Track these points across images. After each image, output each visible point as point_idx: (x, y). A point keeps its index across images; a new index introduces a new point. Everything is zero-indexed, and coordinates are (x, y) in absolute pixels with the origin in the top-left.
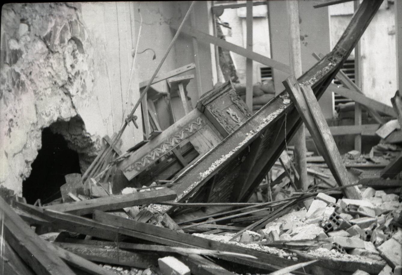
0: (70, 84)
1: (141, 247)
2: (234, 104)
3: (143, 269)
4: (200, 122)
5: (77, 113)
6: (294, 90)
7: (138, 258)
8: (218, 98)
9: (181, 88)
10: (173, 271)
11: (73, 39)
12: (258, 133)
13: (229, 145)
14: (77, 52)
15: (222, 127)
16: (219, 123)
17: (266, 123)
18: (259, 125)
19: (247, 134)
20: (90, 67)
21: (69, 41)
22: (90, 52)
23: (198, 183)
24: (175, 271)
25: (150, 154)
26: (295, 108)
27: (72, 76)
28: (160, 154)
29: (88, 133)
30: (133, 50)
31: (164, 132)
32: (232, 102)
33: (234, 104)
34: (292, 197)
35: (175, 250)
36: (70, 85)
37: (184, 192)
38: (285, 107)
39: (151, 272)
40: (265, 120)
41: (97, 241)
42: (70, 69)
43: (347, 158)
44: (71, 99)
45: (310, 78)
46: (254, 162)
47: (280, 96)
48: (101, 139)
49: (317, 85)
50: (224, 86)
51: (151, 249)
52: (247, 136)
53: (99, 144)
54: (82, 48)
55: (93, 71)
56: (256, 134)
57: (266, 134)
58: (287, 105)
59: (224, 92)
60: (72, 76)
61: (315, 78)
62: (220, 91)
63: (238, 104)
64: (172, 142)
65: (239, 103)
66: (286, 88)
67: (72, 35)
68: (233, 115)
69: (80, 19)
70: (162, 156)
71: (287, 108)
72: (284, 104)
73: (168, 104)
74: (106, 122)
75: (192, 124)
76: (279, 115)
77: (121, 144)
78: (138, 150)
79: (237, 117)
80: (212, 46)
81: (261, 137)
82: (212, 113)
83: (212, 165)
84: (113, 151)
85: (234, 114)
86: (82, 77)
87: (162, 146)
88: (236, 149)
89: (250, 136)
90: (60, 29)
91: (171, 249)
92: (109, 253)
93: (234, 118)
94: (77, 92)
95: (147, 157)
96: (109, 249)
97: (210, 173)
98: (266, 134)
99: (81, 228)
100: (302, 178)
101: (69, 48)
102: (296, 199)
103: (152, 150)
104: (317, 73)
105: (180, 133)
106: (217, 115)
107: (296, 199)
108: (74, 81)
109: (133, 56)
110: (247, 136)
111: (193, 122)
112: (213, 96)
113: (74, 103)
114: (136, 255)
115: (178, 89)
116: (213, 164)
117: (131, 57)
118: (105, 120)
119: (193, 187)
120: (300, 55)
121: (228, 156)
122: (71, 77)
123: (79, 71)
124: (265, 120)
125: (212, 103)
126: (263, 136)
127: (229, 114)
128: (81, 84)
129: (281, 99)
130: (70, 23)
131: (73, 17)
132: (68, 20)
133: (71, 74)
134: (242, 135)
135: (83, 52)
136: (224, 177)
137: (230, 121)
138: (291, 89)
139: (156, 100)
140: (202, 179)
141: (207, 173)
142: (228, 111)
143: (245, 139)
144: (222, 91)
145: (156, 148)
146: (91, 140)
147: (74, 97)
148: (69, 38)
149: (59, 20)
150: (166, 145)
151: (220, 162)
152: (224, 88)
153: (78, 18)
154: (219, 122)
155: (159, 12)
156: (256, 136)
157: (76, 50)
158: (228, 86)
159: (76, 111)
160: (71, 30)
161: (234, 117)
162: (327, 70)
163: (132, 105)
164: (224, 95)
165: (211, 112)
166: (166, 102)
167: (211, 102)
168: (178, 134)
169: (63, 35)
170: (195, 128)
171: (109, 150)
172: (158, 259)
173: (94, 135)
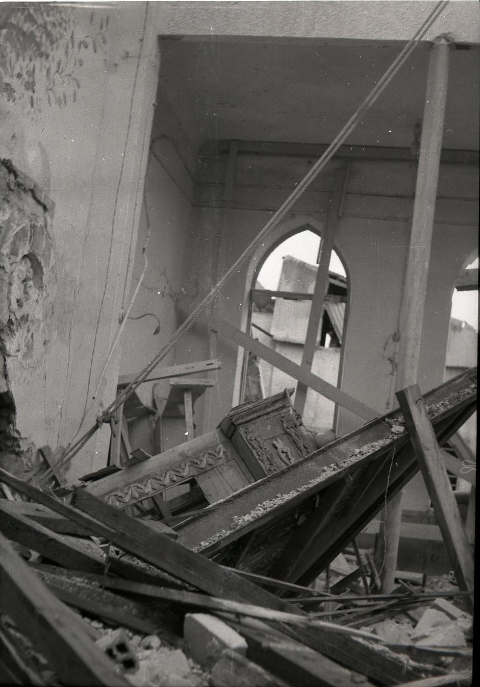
0: (9, 332)
1: (148, 590)
2: (286, 433)
3: (145, 634)
4: (222, 452)
5: (8, 388)
6: (414, 410)
7: (134, 611)
8: (260, 419)
9: (188, 398)
10: (214, 639)
11: (30, 257)
12: (345, 470)
13: (292, 481)
14: (31, 283)
15: (262, 468)
16: (256, 459)
17: (359, 456)
18: (345, 457)
19: (325, 468)
20: (45, 316)
21: (25, 257)
22: (52, 291)
23: (228, 533)
24: (217, 638)
25: (122, 491)
26: (409, 443)
27: (16, 319)
28: (141, 494)
29: (18, 432)
30: (122, 311)
31: (153, 458)
32: (285, 430)
33: (286, 433)
34: (392, 596)
35: (220, 604)
36: (8, 335)
37: (202, 543)
38: (395, 438)
39: (160, 643)
40: (357, 451)
41: (54, 567)
42: (14, 306)
43: (447, 581)
44: (5, 360)
45: (440, 402)
46: (310, 541)
47: (387, 419)
48: (35, 451)
49: (447, 416)
50: (274, 399)
51: (169, 597)
52: (324, 471)
53: (30, 460)
54: (42, 279)
55: (49, 326)
56: (340, 470)
57: (355, 475)
58: (398, 434)
59: (273, 411)
60: (16, 319)
61: (447, 403)
62: (266, 407)
63: (293, 434)
64: (165, 477)
65: (296, 434)
66: (400, 404)
67: (31, 249)
68: (283, 452)
69: (49, 228)
70: (143, 498)
71: (397, 440)
72: (393, 432)
73: (154, 428)
74: (50, 424)
75: (207, 454)
76: (383, 448)
77: (67, 469)
78: (102, 480)
79: (290, 457)
80: (241, 351)
81: (347, 480)
82: (248, 440)
83: (257, 508)
84: (54, 478)
85: (285, 450)
86: (30, 328)
87: (147, 482)
88: (303, 489)
89: (329, 473)
90: (16, 229)
91: (212, 601)
92: (80, 588)
93: (283, 456)
94: (18, 351)
95: (115, 495)
96: (80, 582)
97: (253, 520)
98: (355, 475)
99: (29, 534)
100: (384, 587)
101: (20, 271)
102: (396, 601)
103: (128, 485)
104: (451, 395)
105: (183, 465)
106: (256, 445)
107: (396, 601)
108: (17, 330)
109: (121, 322)
110: (324, 471)
111: (210, 452)
112: (254, 412)
113: (8, 367)
114: (132, 604)
115: (183, 403)
116: (259, 505)
117: (118, 322)
118: (48, 419)
119: (220, 538)
120: (416, 368)
121: (287, 497)
122: (14, 320)
123: (28, 315)
124: (357, 451)
125: (248, 425)
126: (351, 479)
127: (276, 448)
128: (26, 340)
129: (387, 425)
130: (33, 227)
131: (38, 219)
132: (31, 221)
133: (15, 315)
134: (316, 468)
135: (41, 287)
136: (262, 548)
137: (277, 460)
138: (410, 406)
139: (133, 418)
140: (238, 528)
141: (247, 518)
142: (275, 442)
143: (319, 476)
144: (269, 407)
145: (134, 482)
146: (19, 446)
147: (11, 358)
148: (26, 252)
149: (16, 214)
150: (154, 481)
151: (272, 505)
152: (274, 403)
153: (46, 226)
154: (257, 457)
155: (164, 274)
156: (340, 473)
157: (31, 280)
158: (280, 402)
159: (7, 385)
160: (32, 240)
161: (285, 454)
162: (468, 393)
163: (101, 405)
164: (272, 414)
165: (245, 439)
166: (150, 424)
167: (246, 422)
168: (180, 466)
169: (17, 242)
170: (211, 461)
171: (45, 475)
172: (185, 613)
173: (26, 438)
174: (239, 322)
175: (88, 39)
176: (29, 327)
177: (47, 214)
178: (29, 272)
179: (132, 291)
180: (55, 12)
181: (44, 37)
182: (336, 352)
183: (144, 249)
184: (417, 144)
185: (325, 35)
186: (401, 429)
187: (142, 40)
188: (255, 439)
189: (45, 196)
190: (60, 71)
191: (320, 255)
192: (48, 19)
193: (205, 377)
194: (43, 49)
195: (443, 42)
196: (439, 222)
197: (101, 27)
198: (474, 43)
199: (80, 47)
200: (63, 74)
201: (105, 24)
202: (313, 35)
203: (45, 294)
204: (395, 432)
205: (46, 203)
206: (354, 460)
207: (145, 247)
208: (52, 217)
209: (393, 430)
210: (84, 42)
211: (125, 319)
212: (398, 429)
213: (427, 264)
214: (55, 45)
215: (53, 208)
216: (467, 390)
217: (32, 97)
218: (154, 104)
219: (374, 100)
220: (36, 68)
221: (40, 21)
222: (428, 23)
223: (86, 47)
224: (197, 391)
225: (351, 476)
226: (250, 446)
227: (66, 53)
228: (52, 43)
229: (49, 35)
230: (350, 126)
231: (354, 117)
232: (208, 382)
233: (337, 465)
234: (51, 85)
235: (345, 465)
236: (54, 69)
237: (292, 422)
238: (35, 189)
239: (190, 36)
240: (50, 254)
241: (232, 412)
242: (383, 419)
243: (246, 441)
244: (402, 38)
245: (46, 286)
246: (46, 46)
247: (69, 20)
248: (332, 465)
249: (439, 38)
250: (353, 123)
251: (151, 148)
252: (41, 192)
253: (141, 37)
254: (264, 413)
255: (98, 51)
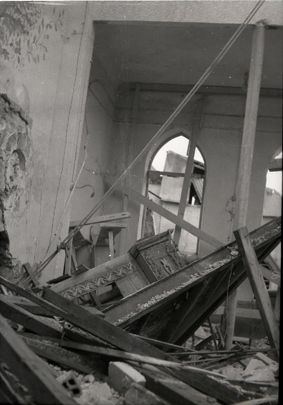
0: (5, 196)
1: (88, 348)
2: (169, 255)
3: (86, 374)
4: (131, 267)
5: (5, 229)
6: (244, 242)
7: (79, 360)
8: (153, 247)
9: (111, 235)
10: (126, 377)
11: (18, 152)
12: (203, 277)
13: (172, 283)
14: (18, 167)
15: (154, 276)
16: (151, 271)
17: (212, 269)
18: (204, 270)
19: (192, 276)
20: (27, 186)
21: (15, 151)
22: (31, 171)
23: (135, 314)
24: (128, 376)
25: (72, 289)
26: (241, 261)
27: (10, 188)
28: (83, 291)
29: (10, 255)
30: (72, 183)
31: (90, 270)
32: (168, 254)
33: (169, 255)
34: (231, 351)
35: (130, 356)
36: (5, 197)
37: (119, 320)
38: (233, 258)
39: (94, 379)
40: (211, 266)
41: (32, 334)
42: (9, 180)
43: (264, 343)
44: (3, 212)
45: (259, 237)
46: (183, 319)
47: (228, 247)
48: (20, 266)
49: (264, 245)
50: (162, 235)
51: (100, 352)
52: (191, 278)
53: (18, 271)
54: (25, 164)
55: (29, 192)
56: (200, 277)
57: (209, 280)
58: (234, 256)
59: (161, 242)
60: (10, 188)
61: (263, 237)
62: (157, 240)
63: (173, 256)
64: (97, 281)
65: (174, 256)
66: (236, 238)
67: (18, 147)
68: (167, 266)
69: (29, 134)
70: (84, 294)
71: (234, 259)
72: (232, 255)
73: (91, 253)
74: (30, 250)
75: (122, 268)
76: (226, 264)
77: (39, 276)
78: (60, 283)
79: (171, 269)
80: (142, 207)
81: (205, 283)
82: (146, 260)
83: (152, 299)
84: (32, 282)
85: (168, 265)
86: (18, 193)
87: (87, 284)
88: (179, 288)
89: (194, 279)
90: (9, 135)
91: (125, 354)
92: (47, 347)
93: (167, 269)
94: (11, 207)
95: (68, 292)
96: (47, 343)
97: (149, 306)
98: (209, 280)
99: (17, 315)
100: (227, 346)
101: (12, 160)
102: (234, 354)
103: (75, 286)
104: (266, 233)
105: (108, 274)
106: (151, 263)
107: (234, 354)
108: (10, 195)
109: (71, 190)
110: (191, 278)
111: (124, 266)
112: (150, 243)
113: (5, 216)
114: (78, 356)
115: (108, 238)
116: (153, 298)
117: (69, 190)
118: (28, 247)
119: (130, 317)
120: (245, 217)
121: (169, 293)
122: (8, 189)
123: (16, 186)
124: (211, 266)
125: (146, 251)
126: (207, 283)
127: (163, 264)
128: (16, 201)
129: (228, 250)
130: (19, 134)
131: (23, 129)
132: (18, 130)
133: (9, 186)
134: (186, 276)
135: (24, 169)
136: (154, 323)
137: (163, 271)
138: (242, 240)
139: (78, 247)
140: (140, 311)
141: (146, 305)
142: (162, 261)
143: (188, 281)
144: (159, 240)
145: (79, 284)
146: (11, 263)
147: (6, 211)
148: (15, 149)
149: (10, 126)
150: (91, 283)
151: (160, 298)
152: (162, 237)
153: (27, 133)
154: (152, 269)
155: (97, 161)
156: (200, 279)
157: (18, 165)
158: (165, 237)
159: (4, 227)
160: (19, 141)
161: (168, 268)
162: (276, 232)
163: (60, 239)
164: (161, 244)
165: (145, 259)
166: (89, 250)
167: (145, 249)
168: (106, 275)
169: (10, 143)
170: (124, 272)
171: (27, 280)
172: (109, 362)
173: (15, 258)
174: (141, 190)
175: (52, 23)
176: (17, 193)
177: (27, 126)
178: (17, 160)
179: (78, 172)
180: (32, 7)
181: (26, 22)
182: (198, 207)
183: (85, 147)
184: (246, 85)
185: (192, 20)
186: (236, 253)
187: (83, 24)
188: (150, 259)
189: (27, 116)
190: (35, 42)
191: (189, 150)
192: (28, 11)
193: (121, 222)
194: (25, 29)
195: (261, 25)
196: (259, 131)
197: (60, 16)
198: (279, 26)
199: (47, 28)
200: (37, 44)
201: (62, 14)
202: (185, 20)
203: (26, 173)
204: (233, 255)
205: (27, 120)
206: (209, 271)
207: (86, 145)
208: (31, 128)
209: (232, 253)
210: (49, 25)
211: (74, 188)
212: (234, 253)
213: (252, 156)
214: (32, 27)
215: (31, 123)
216: (275, 230)
217: (19, 57)
218: (91, 62)
219: (220, 59)
220: (21, 40)
221: (24, 13)
222: (253, 14)
223: (51, 28)
224: (116, 231)
225: (207, 280)
226: (147, 263)
227: (39, 31)
228: (31, 25)
229: (29, 20)
230: (207, 74)
231: (209, 69)
232: (123, 225)
233: (199, 274)
234: (30, 50)
235: (204, 274)
236: (32, 41)
237: (172, 249)
238: (21, 112)
239: (112, 21)
240: (29, 149)
241: (137, 243)
242: (226, 247)
243: (145, 260)
244: (237, 22)
245: (27, 169)
246: (27, 27)
247: (41, 12)
248: (196, 274)
249: (259, 22)
250: (208, 73)
251: (89, 87)
252: (24, 113)
253: (83, 22)
254: (156, 243)
255: (58, 30)
